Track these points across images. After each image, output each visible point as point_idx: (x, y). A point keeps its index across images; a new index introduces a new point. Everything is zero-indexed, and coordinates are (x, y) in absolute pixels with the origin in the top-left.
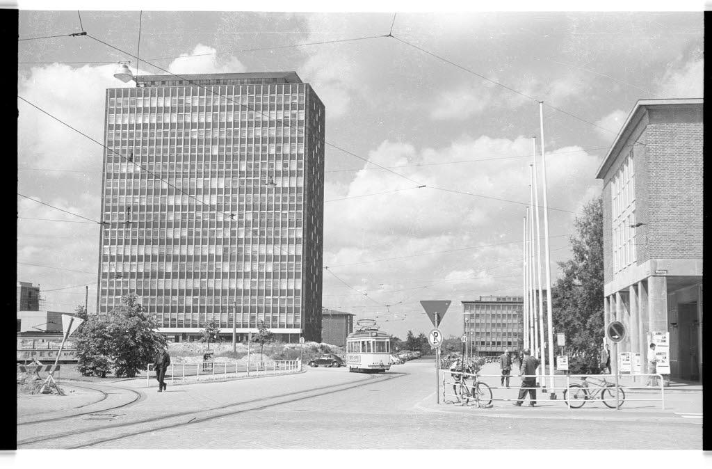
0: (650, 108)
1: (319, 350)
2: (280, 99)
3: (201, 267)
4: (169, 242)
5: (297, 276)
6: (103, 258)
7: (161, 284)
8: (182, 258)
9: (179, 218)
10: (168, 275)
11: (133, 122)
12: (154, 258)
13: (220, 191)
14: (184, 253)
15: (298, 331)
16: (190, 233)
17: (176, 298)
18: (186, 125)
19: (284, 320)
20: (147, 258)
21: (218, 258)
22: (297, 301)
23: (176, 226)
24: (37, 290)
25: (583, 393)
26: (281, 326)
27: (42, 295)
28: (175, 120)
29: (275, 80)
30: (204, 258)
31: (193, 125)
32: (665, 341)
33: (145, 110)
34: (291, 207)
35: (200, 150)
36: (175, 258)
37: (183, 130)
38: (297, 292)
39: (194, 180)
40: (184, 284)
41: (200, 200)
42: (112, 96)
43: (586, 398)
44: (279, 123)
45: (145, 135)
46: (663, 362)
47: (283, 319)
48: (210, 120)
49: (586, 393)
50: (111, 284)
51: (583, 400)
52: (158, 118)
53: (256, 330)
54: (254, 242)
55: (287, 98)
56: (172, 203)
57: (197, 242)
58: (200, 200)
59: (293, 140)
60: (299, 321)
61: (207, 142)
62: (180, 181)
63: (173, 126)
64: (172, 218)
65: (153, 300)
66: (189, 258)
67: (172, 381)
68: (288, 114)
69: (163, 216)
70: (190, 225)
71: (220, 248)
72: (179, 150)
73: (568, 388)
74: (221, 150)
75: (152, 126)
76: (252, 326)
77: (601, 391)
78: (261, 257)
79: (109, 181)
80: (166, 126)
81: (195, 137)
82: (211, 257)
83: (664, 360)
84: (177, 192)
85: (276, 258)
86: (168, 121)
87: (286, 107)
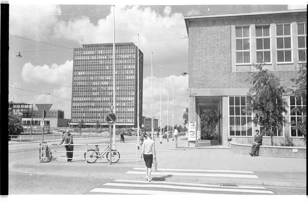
0: (190, 20)
1: (130, 130)
2: (127, 51)
3: (103, 104)
4: (93, 96)
5: (133, 107)
6: (73, 102)
7: (91, 110)
8: (97, 101)
9: (96, 89)
10: (93, 107)
11: (82, 59)
12: (89, 101)
13: (109, 80)
14: (98, 100)
15: (133, 124)
16: (100, 94)
17: (95, 114)
18: (99, 60)
19: (129, 121)
20: (86, 101)
21: (108, 101)
22: (133, 115)
23: (95, 91)
24: (63, 112)
25: (96, 155)
26: (128, 123)
27: (65, 114)
28: (95, 58)
29: (126, 45)
30: (104, 101)
31: (101, 60)
32: (194, 126)
33: (86, 55)
34: (131, 85)
35: (103, 67)
36: (95, 101)
37: (97, 61)
38: (133, 112)
39: (101, 77)
40: (97, 110)
41: (103, 83)
42: (76, 51)
43: (97, 157)
44: (127, 59)
45: (86, 63)
46: (193, 135)
47: (129, 120)
48: (106, 58)
49: (97, 155)
50: (75, 110)
51: (96, 158)
52: (90, 58)
53: (95, 124)
54: (119, 96)
55: (129, 51)
56: (94, 84)
57: (102, 96)
58: (103, 83)
59: (131, 64)
60: (133, 121)
61: (105, 65)
62: (97, 77)
63: (94, 60)
64: (94, 89)
65: (88, 115)
66: (99, 101)
67: (20, 142)
68: (130, 56)
69: (91, 88)
70: (100, 91)
71: (109, 98)
72: (96, 67)
73: (86, 152)
74: (109, 67)
75: (88, 60)
76: (94, 123)
77: (106, 153)
78: (122, 101)
79: (75, 77)
80: (92, 60)
81: (101, 63)
82: (106, 101)
83: (194, 134)
84: (96, 81)
85: (126, 101)
86: (93, 58)
87: (129, 54)
